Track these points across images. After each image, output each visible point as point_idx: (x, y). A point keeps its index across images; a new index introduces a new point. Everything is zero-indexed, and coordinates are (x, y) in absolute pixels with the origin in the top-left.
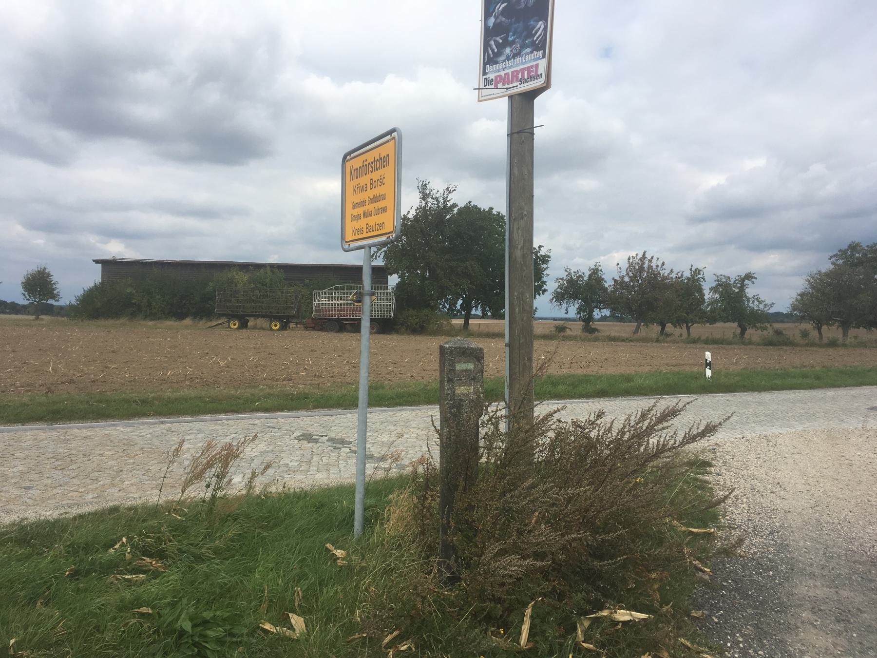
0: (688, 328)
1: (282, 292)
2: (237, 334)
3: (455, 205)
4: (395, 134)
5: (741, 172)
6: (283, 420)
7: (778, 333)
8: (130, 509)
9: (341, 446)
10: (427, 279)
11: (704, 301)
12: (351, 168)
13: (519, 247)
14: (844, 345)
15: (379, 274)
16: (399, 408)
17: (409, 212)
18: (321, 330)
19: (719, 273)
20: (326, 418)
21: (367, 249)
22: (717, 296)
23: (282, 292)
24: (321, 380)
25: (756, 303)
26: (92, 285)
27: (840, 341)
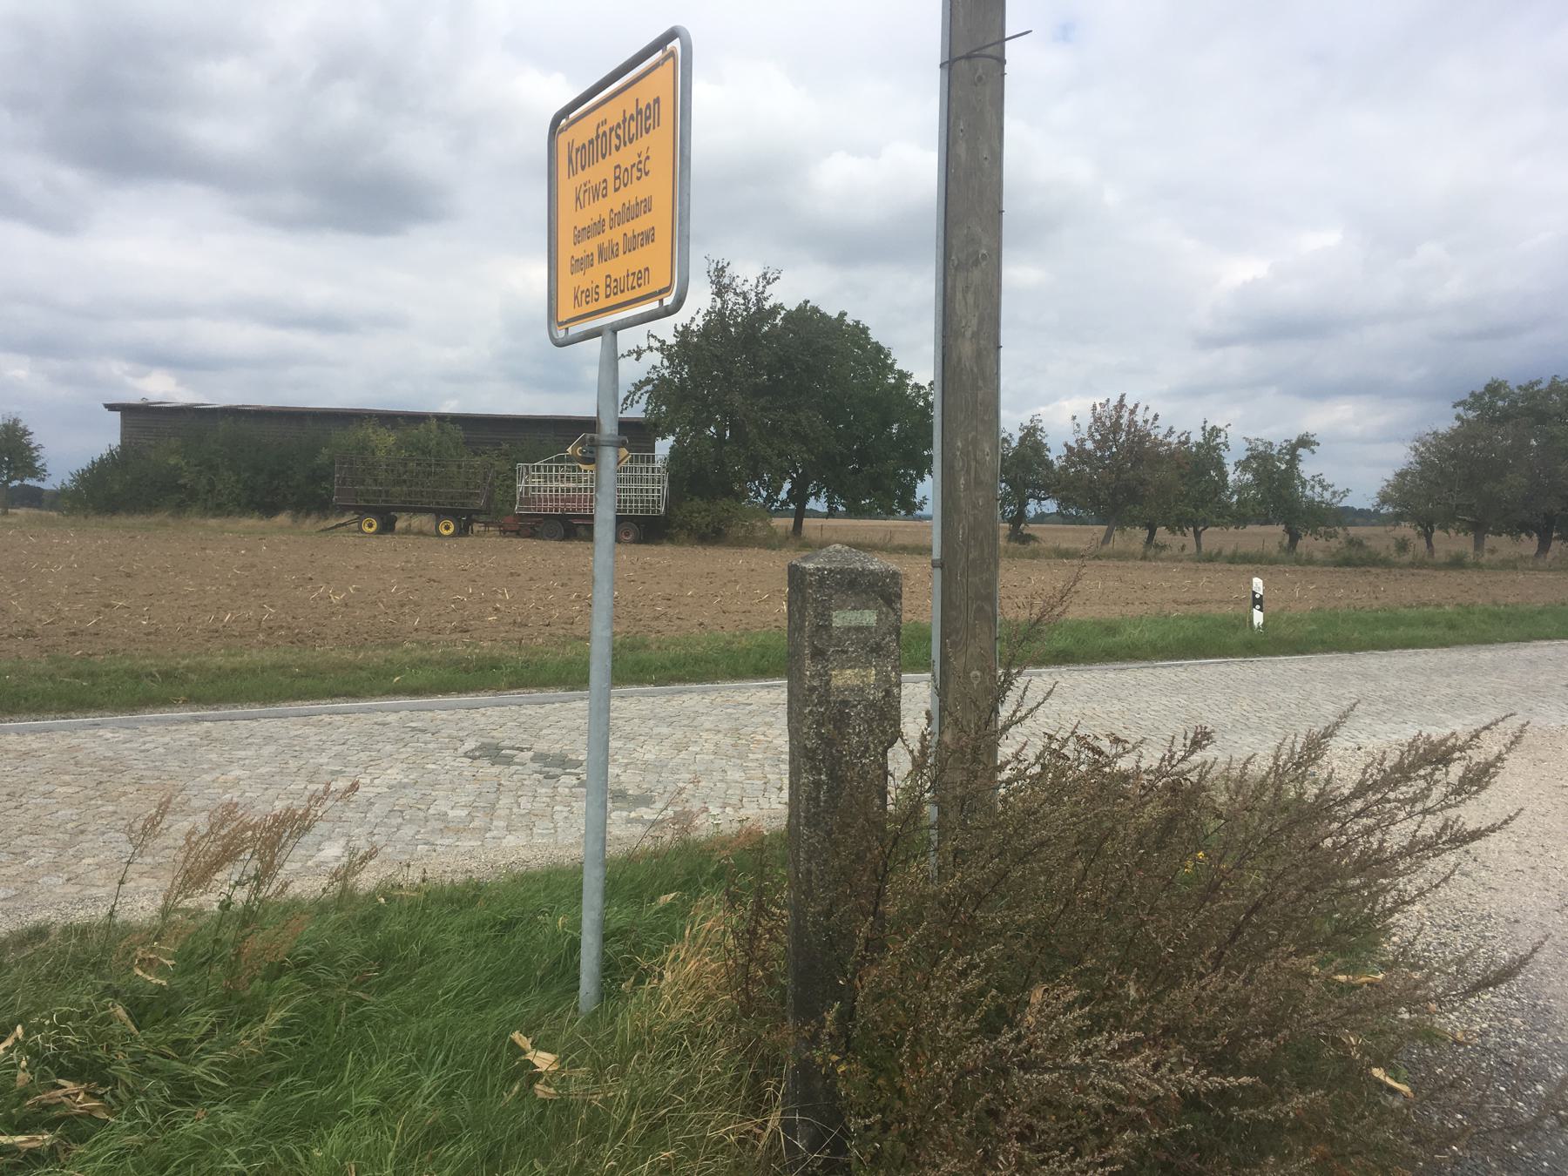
0: (1197, 535)
1: (459, 467)
2: (374, 542)
3: (775, 309)
4: (676, 44)
5: (1295, 256)
6: (444, 715)
7: (1354, 543)
8: (67, 931)
9: (559, 771)
10: (725, 442)
11: (1226, 486)
12: (570, 146)
13: (968, 334)
14: (1477, 566)
15: (637, 435)
16: (678, 687)
17: (693, 319)
18: (533, 535)
19: (1252, 436)
20: (530, 710)
21: (609, 335)
22: (1249, 476)
23: (459, 467)
24: (525, 631)
25: (1318, 489)
26: (105, 452)
27: (1470, 558)
